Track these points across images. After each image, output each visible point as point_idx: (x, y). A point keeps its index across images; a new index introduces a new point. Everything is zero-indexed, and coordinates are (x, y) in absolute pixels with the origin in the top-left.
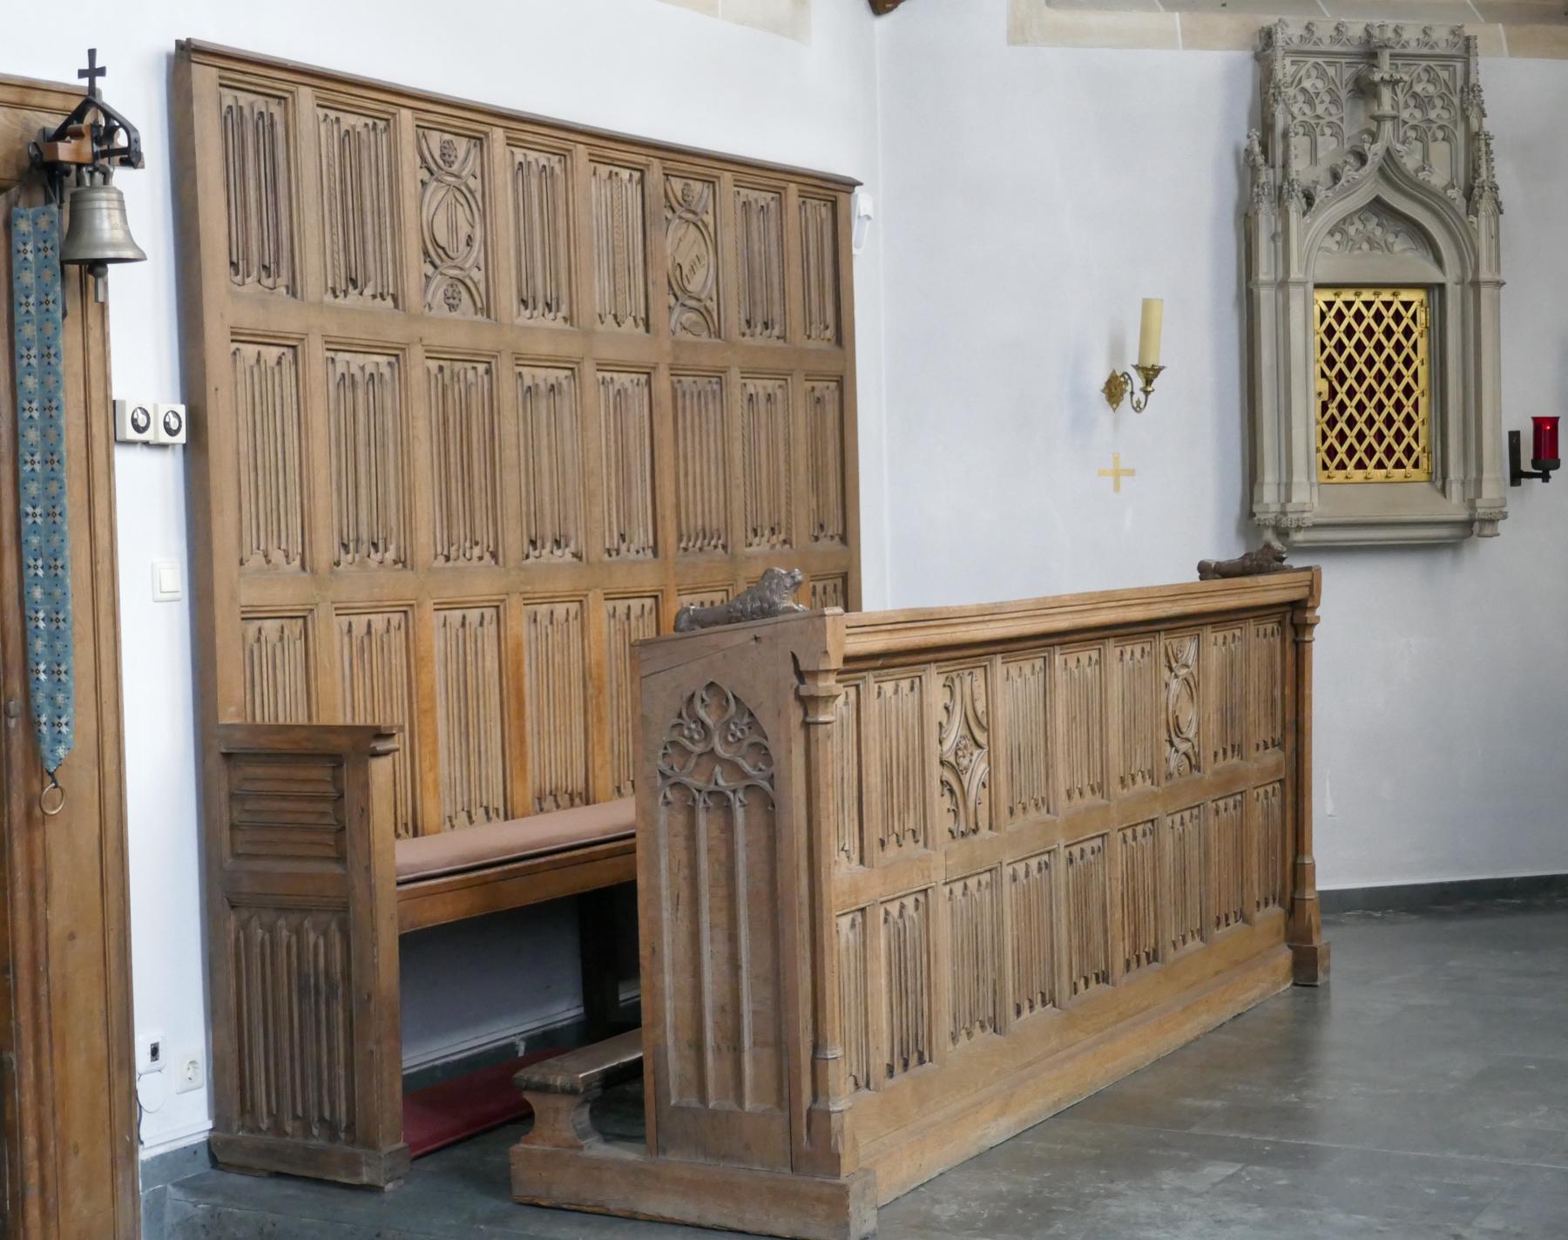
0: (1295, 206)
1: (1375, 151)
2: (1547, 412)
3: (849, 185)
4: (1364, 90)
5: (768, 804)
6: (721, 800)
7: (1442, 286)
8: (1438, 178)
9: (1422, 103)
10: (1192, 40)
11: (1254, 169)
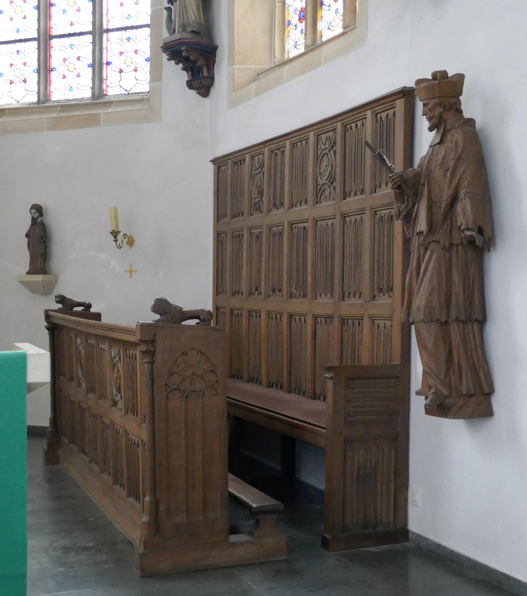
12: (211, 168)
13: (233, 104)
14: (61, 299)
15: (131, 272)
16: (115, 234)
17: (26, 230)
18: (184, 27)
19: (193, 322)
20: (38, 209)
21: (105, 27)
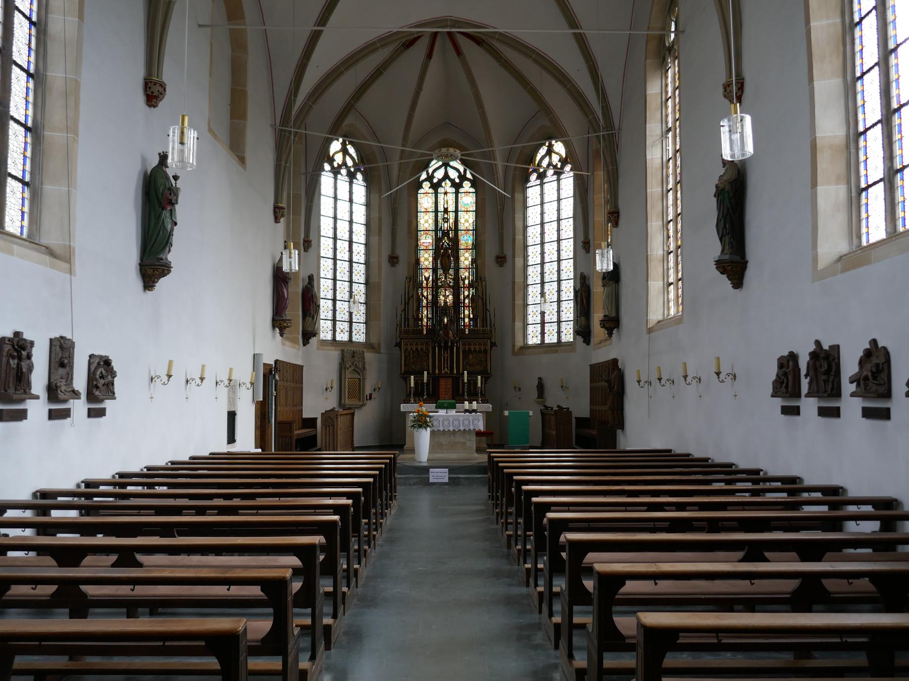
0: (347, 370)
1: (355, 364)
2: (371, 393)
3: (303, 366)
4: (353, 357)
5: (333, 426)
6: (329, 426)
7: (360, 379)
8: (360, 367)
9: (359, 358)
10: (335, 350)
11: (342, 365)
12: (589, 367)
13: (594, 350)
14: (545, 406)
15: (567, 398)
16: (562, 387)
17: (536, 385)
18: (581, 326)
19: (565, 410)
20: (540, 379)
21: (561, 239)
